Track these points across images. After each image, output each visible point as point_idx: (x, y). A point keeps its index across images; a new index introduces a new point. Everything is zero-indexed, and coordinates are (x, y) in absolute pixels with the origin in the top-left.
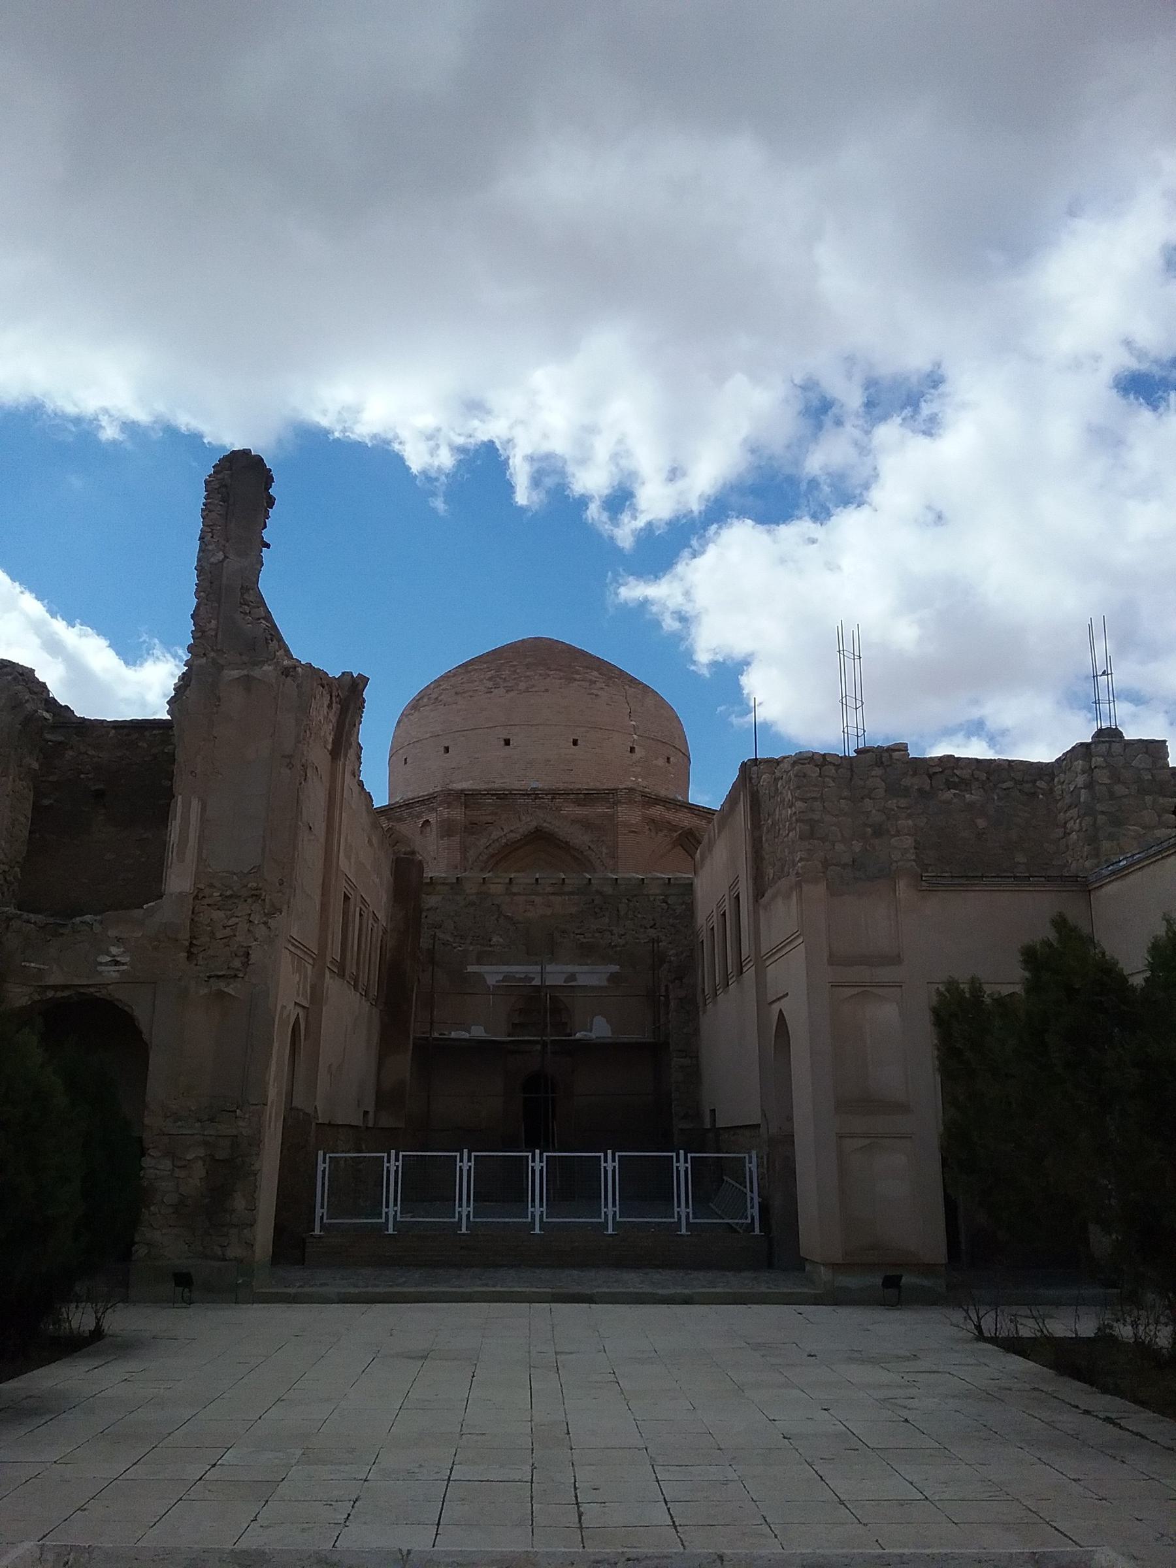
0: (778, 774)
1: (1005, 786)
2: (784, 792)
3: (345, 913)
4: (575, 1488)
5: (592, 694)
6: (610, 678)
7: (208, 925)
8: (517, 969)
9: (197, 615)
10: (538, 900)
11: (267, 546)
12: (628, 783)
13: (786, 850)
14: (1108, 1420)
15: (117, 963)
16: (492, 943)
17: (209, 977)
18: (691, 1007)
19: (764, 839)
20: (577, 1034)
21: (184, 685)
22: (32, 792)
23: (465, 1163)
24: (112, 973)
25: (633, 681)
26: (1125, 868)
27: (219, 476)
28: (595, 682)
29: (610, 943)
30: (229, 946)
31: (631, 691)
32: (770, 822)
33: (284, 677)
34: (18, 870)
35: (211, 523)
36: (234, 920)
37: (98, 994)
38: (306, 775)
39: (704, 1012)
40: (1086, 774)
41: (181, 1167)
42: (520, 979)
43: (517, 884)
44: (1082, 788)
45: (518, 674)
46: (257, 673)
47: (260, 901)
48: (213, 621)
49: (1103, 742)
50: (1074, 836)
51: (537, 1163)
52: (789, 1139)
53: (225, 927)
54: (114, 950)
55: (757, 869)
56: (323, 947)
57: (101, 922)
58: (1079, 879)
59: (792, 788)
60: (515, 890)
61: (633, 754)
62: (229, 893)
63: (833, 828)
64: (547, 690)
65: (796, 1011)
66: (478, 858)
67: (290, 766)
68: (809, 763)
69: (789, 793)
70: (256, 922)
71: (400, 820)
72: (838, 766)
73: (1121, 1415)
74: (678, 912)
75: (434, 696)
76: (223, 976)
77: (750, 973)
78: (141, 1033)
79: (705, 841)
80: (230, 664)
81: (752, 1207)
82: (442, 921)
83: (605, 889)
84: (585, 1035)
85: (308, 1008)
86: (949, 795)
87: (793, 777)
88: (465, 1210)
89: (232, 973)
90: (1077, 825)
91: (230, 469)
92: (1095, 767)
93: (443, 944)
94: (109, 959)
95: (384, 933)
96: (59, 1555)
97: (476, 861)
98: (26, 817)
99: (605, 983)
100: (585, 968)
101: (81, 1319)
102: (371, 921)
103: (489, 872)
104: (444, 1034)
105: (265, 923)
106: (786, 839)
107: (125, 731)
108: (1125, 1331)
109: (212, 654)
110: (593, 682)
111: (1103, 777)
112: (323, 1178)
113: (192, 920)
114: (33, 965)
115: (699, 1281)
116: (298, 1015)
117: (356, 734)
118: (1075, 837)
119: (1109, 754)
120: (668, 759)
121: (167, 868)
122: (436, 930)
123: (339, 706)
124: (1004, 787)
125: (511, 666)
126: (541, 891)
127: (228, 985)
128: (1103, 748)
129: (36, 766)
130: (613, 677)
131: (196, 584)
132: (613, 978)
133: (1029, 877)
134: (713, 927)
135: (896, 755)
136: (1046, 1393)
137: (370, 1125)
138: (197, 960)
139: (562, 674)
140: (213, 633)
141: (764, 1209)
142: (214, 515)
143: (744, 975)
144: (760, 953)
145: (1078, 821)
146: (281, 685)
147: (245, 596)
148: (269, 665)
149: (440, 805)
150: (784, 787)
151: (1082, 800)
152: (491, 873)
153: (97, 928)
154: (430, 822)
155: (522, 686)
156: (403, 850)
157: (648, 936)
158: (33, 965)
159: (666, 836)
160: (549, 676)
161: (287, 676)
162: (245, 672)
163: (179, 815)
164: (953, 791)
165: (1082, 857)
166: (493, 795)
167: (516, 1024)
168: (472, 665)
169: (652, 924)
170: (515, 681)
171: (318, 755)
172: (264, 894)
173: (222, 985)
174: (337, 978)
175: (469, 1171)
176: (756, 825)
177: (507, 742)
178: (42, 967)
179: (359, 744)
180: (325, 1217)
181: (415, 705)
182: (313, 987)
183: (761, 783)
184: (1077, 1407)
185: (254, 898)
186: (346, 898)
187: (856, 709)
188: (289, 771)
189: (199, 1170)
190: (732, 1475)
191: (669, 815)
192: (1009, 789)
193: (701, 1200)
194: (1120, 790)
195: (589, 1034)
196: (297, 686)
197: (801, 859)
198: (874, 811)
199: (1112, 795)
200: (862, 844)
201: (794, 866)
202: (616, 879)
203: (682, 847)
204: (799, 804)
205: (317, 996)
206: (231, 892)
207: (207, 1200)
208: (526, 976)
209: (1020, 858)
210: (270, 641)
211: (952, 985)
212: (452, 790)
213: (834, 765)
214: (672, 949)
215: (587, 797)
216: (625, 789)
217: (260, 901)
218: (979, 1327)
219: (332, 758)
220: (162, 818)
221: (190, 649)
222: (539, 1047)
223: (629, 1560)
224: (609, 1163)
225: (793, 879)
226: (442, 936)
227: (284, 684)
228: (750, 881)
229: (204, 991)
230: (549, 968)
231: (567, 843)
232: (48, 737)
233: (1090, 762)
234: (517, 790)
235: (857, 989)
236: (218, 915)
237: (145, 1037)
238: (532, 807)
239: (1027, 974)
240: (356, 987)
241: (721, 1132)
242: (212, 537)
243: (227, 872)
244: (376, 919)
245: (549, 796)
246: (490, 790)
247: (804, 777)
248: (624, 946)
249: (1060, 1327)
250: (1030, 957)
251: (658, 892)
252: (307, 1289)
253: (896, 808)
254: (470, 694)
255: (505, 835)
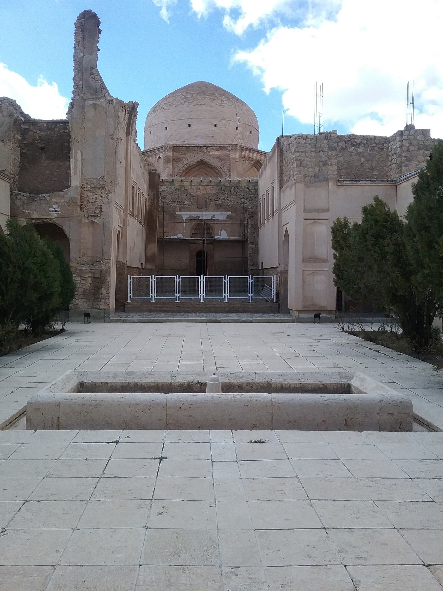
0: (290, 142)
1: (372, 146)
2: (292, 149)
3: (133, 193)
4: (216, 365)
5: (222, 106)
6: (229, 99)
7: (87, 198)
8: (194, 214)
9: (75, 79)
10: (201, 188)
11: (99, 50)
12: (235, 142)
13: (291, 171)
14: (376, 351)
15: (56, 211)
16: (185, 204)
17: (88, 216)
18: (256, 227)
19: (284, 166)
20: (216, 237)
21: (72, 106)
22: (19, 148)
23: (178, 280)
24: (54, 214)
25: (238, 100)
26: (409, 177)
27: (80, 21)
28: (223, 101)
29: (228, 204)
30: (94, 205)
31: (237, 104)
32: (286, 159)
33: (109, 104)
34: (17, 177)
35: (78, 41)
36: (96, 196)
37: (50, 222)
38: (118, 142)
39: (261, 229)
40: (400, 142)
41: (84, 280)
42: (195, 217)
43: (194, 182)
44: (398, 147)
45: (193, 97)
46: (98, 102)
47: (104, 189)
48: (81, 81)
49: (408, 130)
50: (394, 165)
51: (202, 280)
52: (287, 272)
53: (92, 198)
54: (54, 206)
55: (281, 177)
56: (126, 206)
57: (49, 196)
58: (393, 181)
59: (294, 148)
60: (193, 184)
61: (237, 130)
62: (93, 186)
63: (309, 163)
64: (204, 104)
65: (292, 229)
66: (179, 171)
67: (112, 139)
68: (301, 138)
69: (294, 150)
70: (103, 197)
71: (149, 156)
72: (312, 139)
73: (380, 350)
74: (253, 192)
75: (161, 106)
76: (93, 216)
77: (277, 215)
78: (66, 235)
79: (263, 165)
80: (88, 98)
81: (274, 294)
82: (166, 196)
83: (226, 184)
84: (218, 237)
85: (122, 227)
86: (352, 149)
87: (295, 143)
88: (178, 295)
89: (96, 215)
90: (395, 161)
91: (84, 18)
92: (404, 140)
93: (167, 204)
94: (53, 209)
95: (146, 200)
96: (79, 373)
97: (178, 173)
98: (18, 157)
99: (226, 219)
100: (218, 213)
101: (58, 326)
102: (142, 196)
103: (183, 177)
104: (168, 237)
105: (107, 197)
106: (291, 167)
107: (50, 124)
108: (388, 328)
109: (81, 95)
110: (222, 101)
111: (406, 143)
112: (130, 284)
113: (81, 196)
114: (27, 211)
115: (255, 317)
116: (119, 230)
117: (134, 125)
118: (394, 166)
119: (409, 134)
120: (251, 132)
121: (71, 177)
122: (165, 199)
123: (128, 114)
124: (372, 146)
125: (191, 94)
126: (203, 185)
127: (95, 219)
128: (407, 132)
129: (20, 138)
130: (231, 99)
131: (74, 66)
132: (228, 217)
133: (376, 180)
134: (269, 193)
135: (333, 135)
136: (360, 345)
137: (144, 268)
138: (84, 210)
139: (211, 97)
140: (81, 86)
141: (277, 294)
142: (78, 38)
143: (275, 216)
144: (281, 208)
145: (396, 159)
146: (108, 107)
147: (92, 71)
148: (103, 99)
149: (164, 150)
150: (292, 147)
151: (398, 152)
152: (184, 178)
153: (48, 198)
154: (160, 157)
155: (195, 102)
156: (152, 169)
157: (242, 201)
158: (27, 211)
159: (249, 163)
160: (205, 98)
161: (109, 104)
162: (94, 102)
163: (73, 157)
164: (353, 148)
165: (395, 173)
166: (184, 147)
167: (194, 234)
168: (176, 93)
169: (243, 197)
170: (193, 100)
171: (122, 134)
172: (105, 187)
173: (93, 219)
174: (131, 217)
175: (179, 282)
176: (281, 161)
177: (189, 126)
178: (30, 212)
179: (136, 129)
180: (131, 297)
181: (154, 110)
182: (124, 220)
183: (284, 145)
184: (368, 348)
185: (102, 188)
186: (133, 188)
187: (320, 117)
188: (112, 141)
189: (90, 281)
190: (260, 362)
191: (250, 155)
192: (374, 147)
193: (256, 293)
194: (411, 148)
195: (219, 237)
196: (114, 108)
197: (296, 174)
198: (323, 156)
199: (408, 150)
200: (318, 168)
201: (294, 177)
202: (230, 180)
203: (255, 167)
204: (297, 154)
205: (125, 223)
206: (94, 186)
207: (93, 291)
208: (197, 216)
209: (375, 173)
210: (102, 89)
211: (338, 219)
212: (169, 145)
213: (310, 139)
214: (250, 206)
215: (220, 148)
216: (234, 144)
217: (104, 189)
218: (343, 328)
219: (127, 135)
220: (67, 158)
221: (73, 92)
222: (202, 241)
223: (231, 373)
224: (226, 280)
225: (293, 181)
226: (166, 201)
227: (108, 107)
228: (278, 181)
229: (87, 221)
230: (206, 213)
231: (212, 166)
232: (23, 126)
233: (402, 137)
234: (193, 145)
235: (312, 220)
236: (90, 194)
237: (68, 236)
238: (199, 152)
239: (363, 216)
240: (137, 220)
241: (265, 270)
242: (79, 47)
243: (92, 178)
244: (143, 195)
245: (206, 147)
246: (183, 145)
247: (299, 143)
248: (233, 205)
249: (368, 329)
250: (365, 210)
251: (245, 185)
252: (127, 318)
253: (331, 155)
254: (175, 105)
255: (189, 163)
